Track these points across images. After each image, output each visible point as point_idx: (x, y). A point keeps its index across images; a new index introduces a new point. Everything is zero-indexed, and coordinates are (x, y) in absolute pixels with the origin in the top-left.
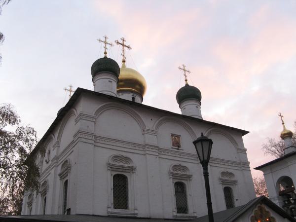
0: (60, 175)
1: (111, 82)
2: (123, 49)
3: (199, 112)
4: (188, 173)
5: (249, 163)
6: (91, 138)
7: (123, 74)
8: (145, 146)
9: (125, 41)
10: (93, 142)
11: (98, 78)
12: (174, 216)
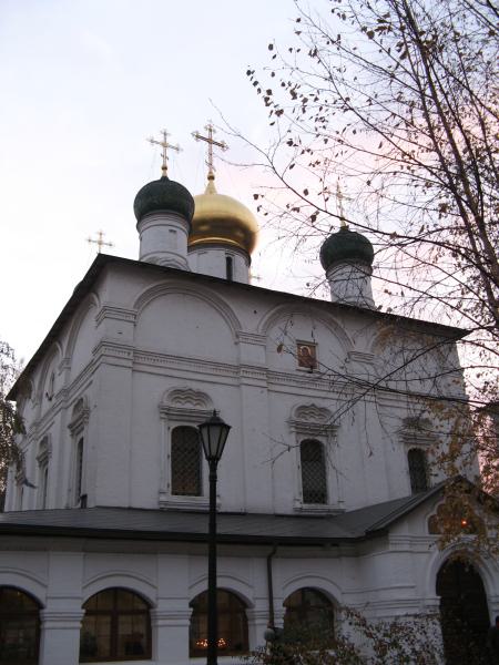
0: (70, 426)
1: (175, 232)
2: (211, 149)
6: (126, 356)
7: (200, 210)
8: (238, 369)
10: (130, 364)
11: (148, 225)
12: (296, 509)
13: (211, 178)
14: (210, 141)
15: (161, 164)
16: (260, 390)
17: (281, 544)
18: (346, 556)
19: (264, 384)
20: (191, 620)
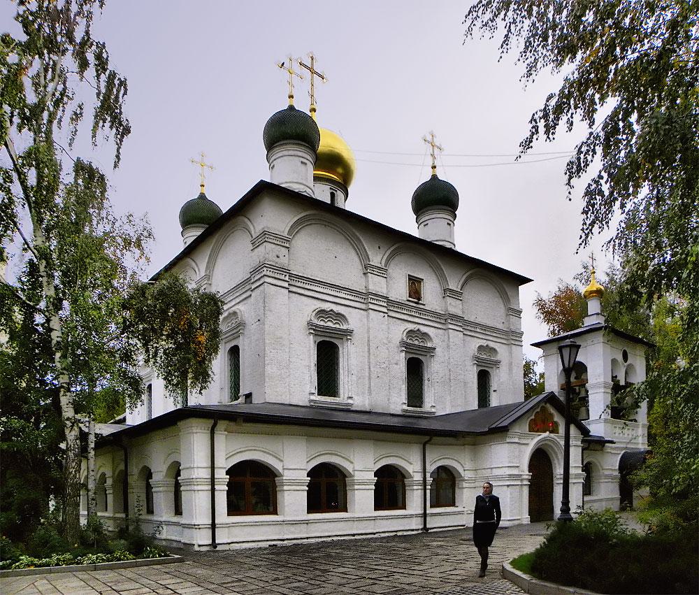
1: (306, 164)
3: (451, 234)
6: (283, 277)
11: (280, 154)
14: (311, 70)
15: (431, 164)
18: (468, 444)
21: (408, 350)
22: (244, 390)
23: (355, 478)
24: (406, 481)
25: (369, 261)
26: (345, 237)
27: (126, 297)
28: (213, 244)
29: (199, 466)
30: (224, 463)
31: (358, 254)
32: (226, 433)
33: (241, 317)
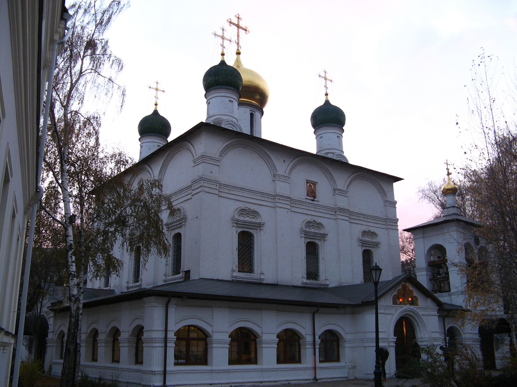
1: (232, 101)
2: (238, 33)
3: (340, 144)
4: (322, 232)
5: (398, 220)
6: (214, 187)
8: (275, 197)
9: (241, 19)
12: (303, 283)
13: (238, 53)
14: (238, 26)
15: (221, 52)
16: (286, 210)
17: (322, 307)
19: (289, 207)
20: (278, 345)
21: (307, 236)
22: (185, 267)
23: (307, 340)
24: (301, 341)
25: (277, 172)
26: (259, 155)
27: (50, 123)
28: (165, 157)
29: (162, 328)
30: (173, 327)
31: (269, 167)
32: (176, 306)
33: (184, 213)
